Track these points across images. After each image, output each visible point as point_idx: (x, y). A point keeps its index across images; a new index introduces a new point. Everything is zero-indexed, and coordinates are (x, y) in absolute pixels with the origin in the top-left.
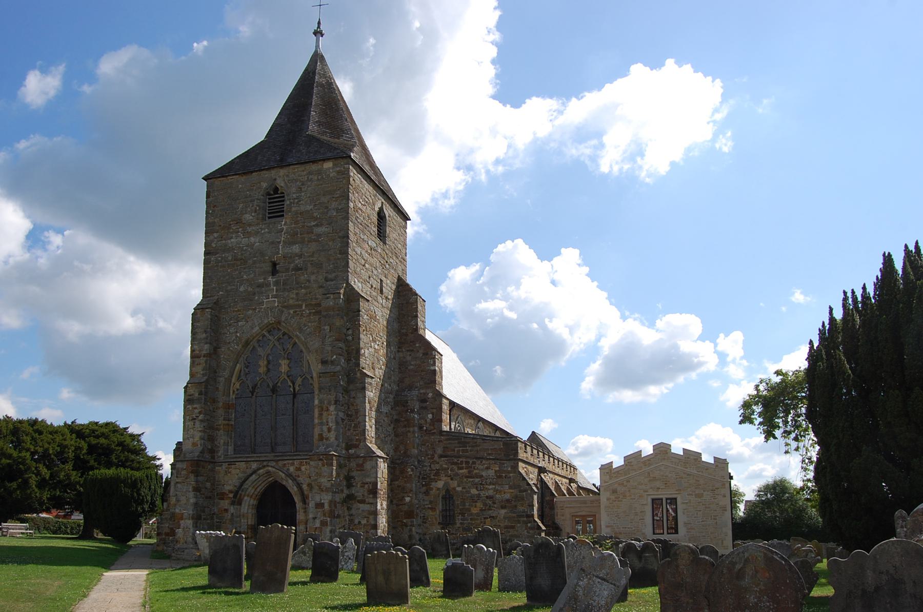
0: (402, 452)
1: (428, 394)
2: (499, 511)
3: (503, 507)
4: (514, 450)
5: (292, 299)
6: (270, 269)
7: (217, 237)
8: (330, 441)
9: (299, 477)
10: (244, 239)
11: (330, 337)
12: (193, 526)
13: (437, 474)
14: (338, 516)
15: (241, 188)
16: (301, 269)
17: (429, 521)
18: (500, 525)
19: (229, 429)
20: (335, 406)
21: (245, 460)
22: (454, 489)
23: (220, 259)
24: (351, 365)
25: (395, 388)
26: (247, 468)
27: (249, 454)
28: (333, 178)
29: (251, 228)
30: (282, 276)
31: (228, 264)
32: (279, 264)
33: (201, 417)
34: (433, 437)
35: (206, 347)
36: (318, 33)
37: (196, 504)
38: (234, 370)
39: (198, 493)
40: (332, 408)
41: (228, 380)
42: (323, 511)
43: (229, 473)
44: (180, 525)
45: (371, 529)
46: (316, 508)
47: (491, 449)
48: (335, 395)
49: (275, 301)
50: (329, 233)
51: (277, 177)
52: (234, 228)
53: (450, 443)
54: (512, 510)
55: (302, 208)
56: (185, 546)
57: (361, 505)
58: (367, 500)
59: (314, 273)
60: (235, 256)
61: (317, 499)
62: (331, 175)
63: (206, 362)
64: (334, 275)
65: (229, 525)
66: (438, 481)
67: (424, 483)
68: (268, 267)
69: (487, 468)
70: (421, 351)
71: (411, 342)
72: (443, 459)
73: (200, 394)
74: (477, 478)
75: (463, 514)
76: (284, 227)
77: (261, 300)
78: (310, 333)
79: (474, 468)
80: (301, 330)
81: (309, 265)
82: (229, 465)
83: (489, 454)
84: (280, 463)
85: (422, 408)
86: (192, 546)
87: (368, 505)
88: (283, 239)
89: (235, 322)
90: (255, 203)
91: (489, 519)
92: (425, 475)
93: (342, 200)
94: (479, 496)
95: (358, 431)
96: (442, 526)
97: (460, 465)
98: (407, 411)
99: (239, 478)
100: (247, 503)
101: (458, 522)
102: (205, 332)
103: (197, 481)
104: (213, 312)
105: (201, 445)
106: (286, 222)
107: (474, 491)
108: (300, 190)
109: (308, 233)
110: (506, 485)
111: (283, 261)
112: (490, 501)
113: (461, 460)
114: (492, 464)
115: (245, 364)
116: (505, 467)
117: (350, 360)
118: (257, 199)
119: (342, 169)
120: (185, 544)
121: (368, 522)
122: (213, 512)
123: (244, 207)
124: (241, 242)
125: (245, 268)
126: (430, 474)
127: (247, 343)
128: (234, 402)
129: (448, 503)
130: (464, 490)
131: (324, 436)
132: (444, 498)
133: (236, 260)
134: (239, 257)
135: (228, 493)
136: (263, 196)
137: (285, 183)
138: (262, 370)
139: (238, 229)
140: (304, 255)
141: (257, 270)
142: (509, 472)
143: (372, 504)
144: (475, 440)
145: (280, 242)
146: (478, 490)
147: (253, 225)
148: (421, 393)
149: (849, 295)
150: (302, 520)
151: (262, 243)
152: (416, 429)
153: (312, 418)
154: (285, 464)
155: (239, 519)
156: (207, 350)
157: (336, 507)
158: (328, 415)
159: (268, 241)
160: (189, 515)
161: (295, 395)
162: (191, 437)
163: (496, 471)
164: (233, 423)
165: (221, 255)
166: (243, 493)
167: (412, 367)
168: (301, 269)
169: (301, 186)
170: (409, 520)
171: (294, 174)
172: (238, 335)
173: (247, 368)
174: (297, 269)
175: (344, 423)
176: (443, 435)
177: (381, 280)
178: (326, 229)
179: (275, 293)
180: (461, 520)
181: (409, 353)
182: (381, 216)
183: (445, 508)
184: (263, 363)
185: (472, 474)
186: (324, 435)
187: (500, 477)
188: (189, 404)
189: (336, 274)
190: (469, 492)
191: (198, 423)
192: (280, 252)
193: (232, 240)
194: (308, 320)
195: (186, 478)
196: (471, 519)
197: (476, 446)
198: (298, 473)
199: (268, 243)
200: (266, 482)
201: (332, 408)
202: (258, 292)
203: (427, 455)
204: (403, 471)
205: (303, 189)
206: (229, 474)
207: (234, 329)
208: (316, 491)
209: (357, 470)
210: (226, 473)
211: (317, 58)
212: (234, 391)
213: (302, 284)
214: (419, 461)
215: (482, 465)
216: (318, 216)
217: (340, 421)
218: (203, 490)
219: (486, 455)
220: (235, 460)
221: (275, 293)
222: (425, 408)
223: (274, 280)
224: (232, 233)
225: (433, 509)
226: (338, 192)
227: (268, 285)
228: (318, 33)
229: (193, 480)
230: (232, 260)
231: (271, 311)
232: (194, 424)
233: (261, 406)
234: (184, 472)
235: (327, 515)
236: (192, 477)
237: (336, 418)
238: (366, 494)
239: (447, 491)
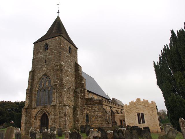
3: (100, 118)
6: (45, 61)
13: (84, 110)
14: (56, 122)
25: (75, 88)
30: (47, 63)
35: (31, 80)
36: (58, 13)
37: (26, 120)
41: (36, 88)
55: (52, 47)
57: (62, 119)
68: (44, 61)
69: (96, 107)
70: (80, 79)
75: (91, 120)
83: (96, 104)
84: (45, 108)
101: (90, 122)
103: (26, 114)
107: (93, 114)
108: (51, 43)
127: (40, 79)
132: (86, 116)
138: (43, 85)
142: (101, 108)
149: (166, 46)
152: (79, 98)
157: (55, 119)
161: (49, 91)
174: (50, 61)
177: (70, 63)
182: (70, 48)
184: (43, 84)
187: (99, 110)
190: (92, 114)
201: (55, 93)
204: (76, 109)
211: (58, 18)
214: (80, 106)
217: (57, 96)
222: (81, 93)
225: (84, 119)
227: (44, 65)
228: (58, 13)
239: (87, 114)
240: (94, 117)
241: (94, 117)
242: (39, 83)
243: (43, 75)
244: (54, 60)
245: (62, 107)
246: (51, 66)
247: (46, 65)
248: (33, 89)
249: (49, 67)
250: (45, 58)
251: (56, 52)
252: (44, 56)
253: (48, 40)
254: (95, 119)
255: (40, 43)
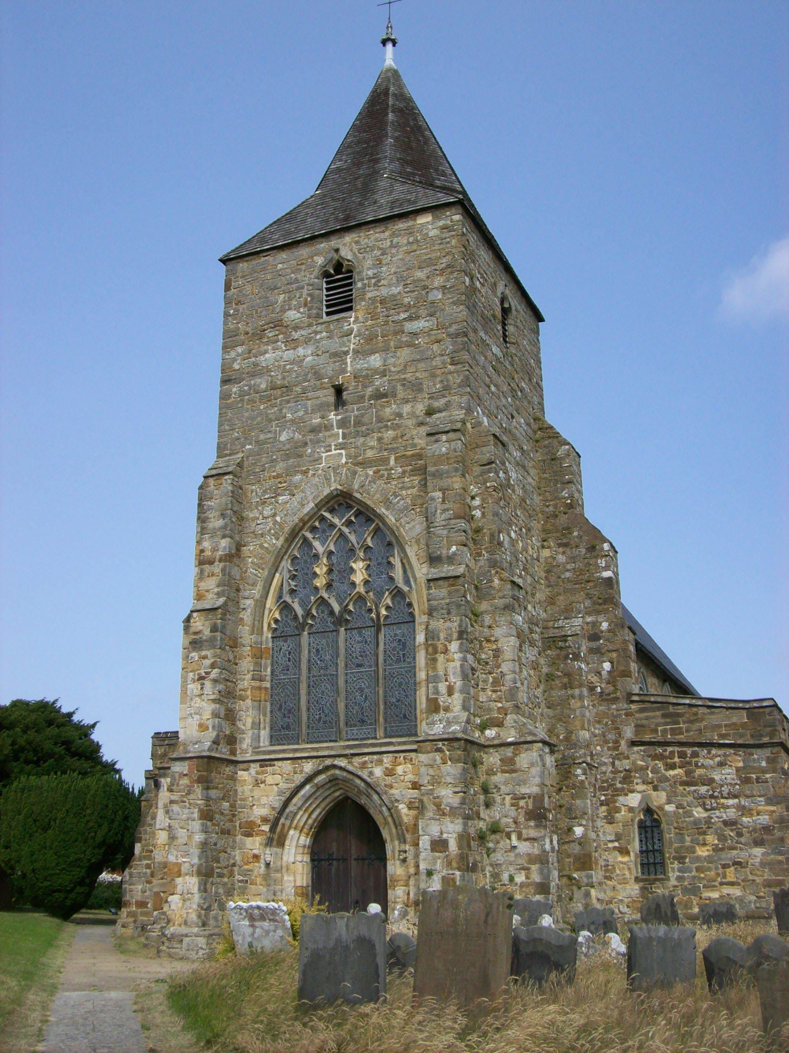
0: (561, 737)
1: (601, 624)
2: (749, 850)
3: (758, 843)
4: (771, 726)
5: (372, 448)
6: (332, 399)
7: (242, 352)
8: (452, 711)
9: (391, 787)
10: (287, 352)
11: (444, 511)
12: (199, 890)
13: (627, 778)
15: (280, 270)
16: (385, 395)
17: (618, 875)
18: (754, 881)
19: (260, 697)
20: (459, 642)
21: (291, 755)
22: (661, 808)
23: (246, 388)
24: (482, 563)
26: (295, 773)
27: (298, 744)
28: (434, 238)
29: (298, 333)
30: (353, 411)
31: (260, 396)
32: (346, 389)
33: (215, 673)
34: (614, 706)
38: (271, 585)
39: (209, 823)
40: (454, 646)
41: (261, 604)
42: (447, 856)
43: (262, 783)
44: (175, 887)
45: (535, 894)
46: (433, 850)
47: (726, 726)
48: (458, 622)
49: (341, 454)
50: (432, 330)
51: (340, 246)
52: (270, 335)
53: (647, 718)
54: (776, 848)
55: (384, 292)
56: (184, 930)
58: (524, 831)
59: (407, 401)
60: (271, 382)
61: (434, 829)
62: (431, 234)
63: (223, 570)
64: (442, 401)
65: (261, 887)
66: (630, 795)
67: (603, 798)
69: (721, 764)
71: (563, 529)
72: (636, 749)
73: (214, 629)
74: (704, 784)
76: (355, 326)
77: (316, 455)
78: (406, 508)
79: (696, 765)
80: (388, 503)
81: (399, 387)
82: (261, 766)
84: (357, 760)
85: (592, 651)
86: (196, 930)
87: (527, 843)
88: (352, 346)
89: (273, 497)
90: (305, 291)
91: (732, 869)
92: (603, 782)
93: (452, 273)
94: (708, 821)
95: (500, 691)
96: (641, 884)
97: (669, 761)
98: (567, 657)
99: (280, 793)
100: (294, 843)
101: (673, 875)
102: (223, 516)
103: (208, 799)
104: (236, 480)
105: (214, 727)
106: (357, 318)
107: (699, 813)
109: (396, 333)
110: (760, 796)
111: (353, 384)
112: (732, 830)
113: (670, 749)
114: (728, 756)
115: (290, 571)
116: (754, 760)
117: (480, 554)
118: (309, 285)
119: (449, 222)
120: (183, 926)
121: (527, 878)
122: (232, 861)
123: (286, 298)
124: (281, 358)
125: (288, 402)
126: (614, 779)
127: (294, 534)
128: (270, 645)
129: (649, 835)
130: (681, 811)
131: (441, 704)
132: (642, 826)
133: (274, 388)
134: (279, 382)
135: (259, 822)
136: (318, 279)
137: (354, 254)
139: (277, 335)
140: (390, 371)
141: (309, 402)
142: (764, 771)
143: (534, 839)
144: (695, 709)
145: (348, 351)
146: (706, 810)
147: (301, 328)
148: (588, 623)
150: (399, 875)
151: (318, 355)
152: (585, 691)
153: (412, 670)
154: (365, 762)
155: (279, 875)
156: (225, 548)
158: (448, 660)
159: (328, 352)
160: (193, 866)
162: (196, 714)
163: (738, 770)
164: (268, 685)
165: (249, 383)
166: (288, 823)
167: (568, 574)
168: (385, 395)
169: (381, 257)
170: (584, 873)
171: (369, 239)
172: (278, 519)
173: (292, 580)
174: (379, 396)
175: (475, 676)
176: (633, 702)
178: (427, 324)
179: (341, 440)
180: (679, 871)
181: (561, 550)
183: (644, 849)
185: (694, 778)
186: (441, 700)
187: (746, 781)
188: (194, 649)
189: (447, 399)
190: (689, 814)
191: (208, 684)
192: (349, 369)
193: (267, 356)
194: (400, 486)
195: (189, 793)
196: (698, 869)
197: (697, 720)
198: (389, 780)
199: (327, 355)
200: (328, 800)
202: (311, 440)
203: (607, 742)
205: (384, 262)
206: (262, 785)
207: (271, 509)
208: (431, 814)
209: (503, 772)
210: (257, 783)
212: (269, 625)
213: (389, 421)
215: (711, 759)
216: (412, 303)
218: (217, 816)
219: (716, 738)
220: (272, 756)
221: (341, 440)
223: (339, 417)
224: (267, 343)
225: (624, 851)
226: (444, 260)
227: (328, 428)
229: (200, 797)
230: (267, 388)
231: (334, 473)
232: (202, 688)
233: (318, 651)
234: (185, 781)
235: (454, 864)
236: (198, 790)
237: (462, 666)
238: (521, 819)
239: (648, 811)
240: (711, 839)
241: (711, 839)
242: (286, 564)
243: (319, 506)
244: (417, 387)
245: (509, 752)
246: (391, 433)
247: (342, 424)
248: (239, 609)
249: (373, 443)
250: (329, 370)
251: (428, 333)
252: (324, 358)
253: (348, 238)
254: (716, 849)
255: (283, 255)
